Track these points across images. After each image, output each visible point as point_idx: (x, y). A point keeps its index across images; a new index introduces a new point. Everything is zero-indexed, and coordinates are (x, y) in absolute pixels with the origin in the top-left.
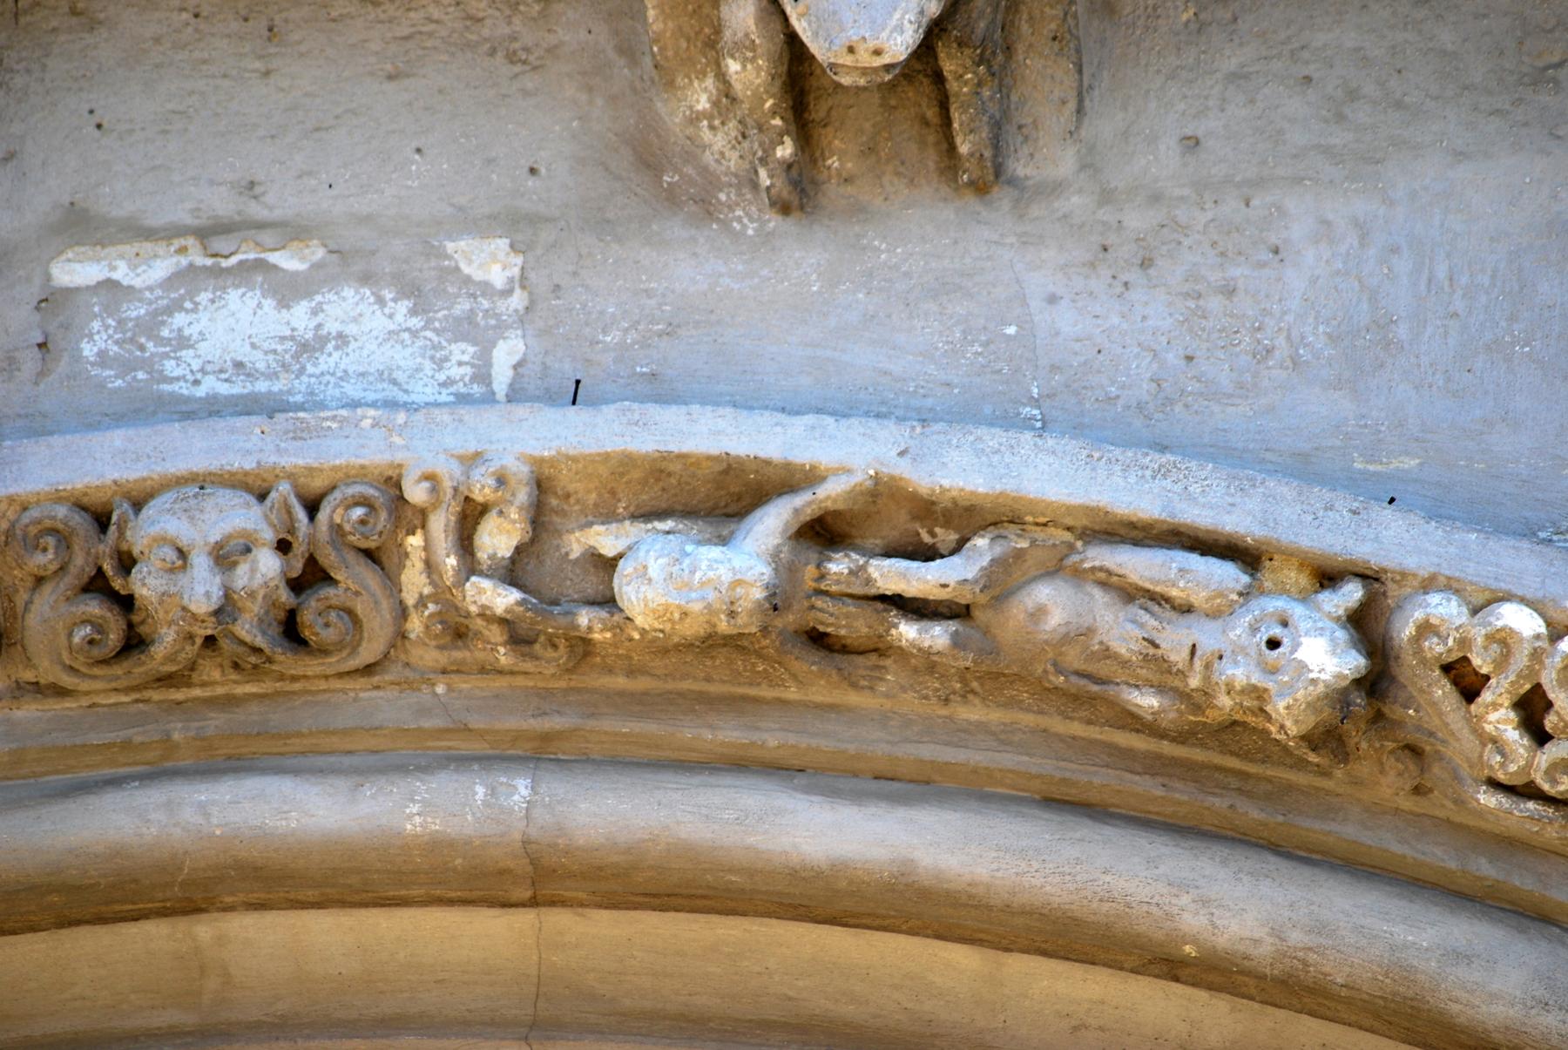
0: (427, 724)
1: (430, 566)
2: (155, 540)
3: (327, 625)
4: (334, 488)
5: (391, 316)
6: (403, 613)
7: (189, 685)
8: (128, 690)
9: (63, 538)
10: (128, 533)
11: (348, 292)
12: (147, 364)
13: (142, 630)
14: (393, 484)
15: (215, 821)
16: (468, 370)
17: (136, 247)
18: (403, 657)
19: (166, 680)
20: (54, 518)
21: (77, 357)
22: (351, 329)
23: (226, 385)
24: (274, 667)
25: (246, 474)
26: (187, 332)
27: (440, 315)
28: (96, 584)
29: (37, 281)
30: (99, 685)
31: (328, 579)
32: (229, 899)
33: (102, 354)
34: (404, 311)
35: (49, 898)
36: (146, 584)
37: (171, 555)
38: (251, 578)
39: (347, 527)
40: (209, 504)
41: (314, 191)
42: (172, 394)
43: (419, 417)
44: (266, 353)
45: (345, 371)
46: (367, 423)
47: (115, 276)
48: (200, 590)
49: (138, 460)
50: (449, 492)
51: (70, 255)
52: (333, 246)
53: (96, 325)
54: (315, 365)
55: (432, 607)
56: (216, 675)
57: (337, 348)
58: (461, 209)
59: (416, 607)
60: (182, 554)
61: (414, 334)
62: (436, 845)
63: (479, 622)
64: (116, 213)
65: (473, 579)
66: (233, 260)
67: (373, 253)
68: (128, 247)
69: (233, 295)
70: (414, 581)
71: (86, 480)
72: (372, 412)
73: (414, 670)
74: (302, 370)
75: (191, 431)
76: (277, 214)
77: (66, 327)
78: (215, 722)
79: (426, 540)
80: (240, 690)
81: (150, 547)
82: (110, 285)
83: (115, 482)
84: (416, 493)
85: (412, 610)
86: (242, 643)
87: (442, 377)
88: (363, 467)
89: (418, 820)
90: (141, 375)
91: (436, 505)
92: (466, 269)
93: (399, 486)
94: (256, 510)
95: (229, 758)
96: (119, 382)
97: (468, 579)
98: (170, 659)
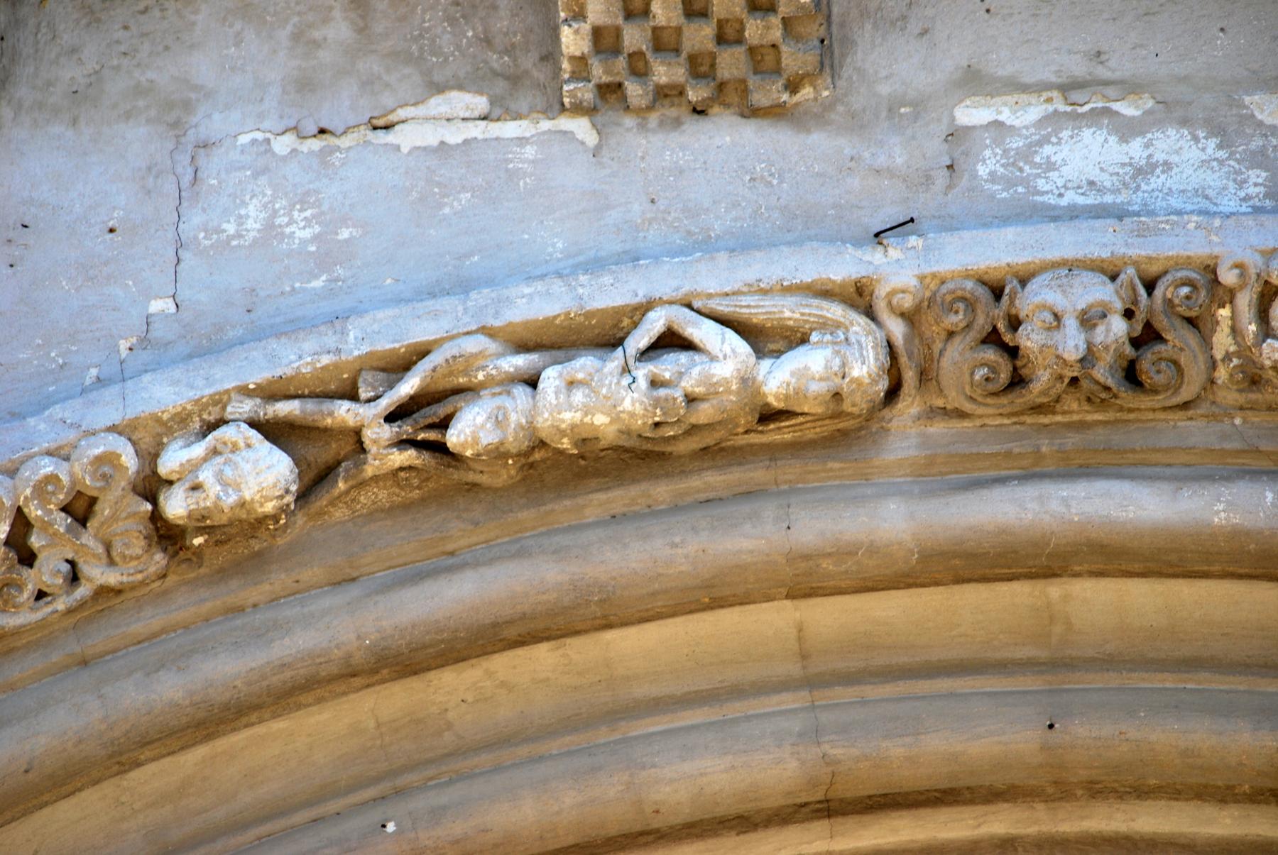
0: (1228, 446)
1: (1235, 331)
2: (1037, 307)
3: (1159, 372)
4: (1166, 273)
5: (1203, 150)
6: (1213, 365)
7: (1054, 413)
8: (1010, 415)
9: (971, 304)
10: (1017, 302)
11: (1171, 132)
12: (1025, 182)
13: (1024, 372)
14: (1210, 270)
15: (1074, 511)
16: (1262, 189)
17: (1016, 97)
18: (1211, 397)
19: (1038, 409)
20: (964, 289)
21: (975, 176)
22: (1174, 159)
23: (1082, 198)
24: (1118, 402)
25: (1103, 261)
26: (1053, 159)
27: (1240, 149)
28: (992, 338)
29: (945, 121)
30: (990, 411)
31: (1159, 338)
32: (1077, 568)
33: (992, 173)
34: (1213, 146)
35: (953, 562)
36: (1030, 339)
37: (1049, 317)
38: (1106, 336)
39: (1176, 301)
40: (1076, 282)
41: (1144, 58)
42: (1043, 203)
43: (1231, 221)
44: (1111, 175)
45: (1170, 189)
46: (1191, 226)
47: (1001, 118)
48: (1071, 343)
49: (1024, 249)
50: (1254, 277)
51: (968, 103)
52: (1159, 99)
53: (988, 153)
54: (1147, 184)
55: (1235, 361)
56: (1075, 406)
57: (1163, 172)
58: (1254, 72)
59: (1223, 360)
60: (1057, 317)
61: (1221, 162)
62: (1236, 534)
63: (1270, 372)
64: (1000, 73)
65: (1269, 341)
66: (1087, 108)
67: (1190, 103)
68: (1009, 98)
69: (1087, 133)
70: (1222, 341)
71: (987, 263)
72: (1195, 218)
73: (1218, 406)
74: (1138, 188)
75: (1062, 229)
76: (1118, 75)
77: (966, 154)
78: (1072, 440)
79: (1233, 312)
80: (1089, 418)
81: (1034, 311)
82: (997, 124)
83: (1008, 265)
84: (1228, 277)
85: (1220, 363)
86: (1098, 383)
87: (1242, 194)
88: (1189, 257)
89: (1223, 515)
90: (1020, 189)
91: (1242, 287)
92: (1259, 116)
93: (1214, 272)
94: (1110, 287)
95: (1081, 466)
96: (1004, 194)
97: (1264, 341)
98: (1044, 393)
